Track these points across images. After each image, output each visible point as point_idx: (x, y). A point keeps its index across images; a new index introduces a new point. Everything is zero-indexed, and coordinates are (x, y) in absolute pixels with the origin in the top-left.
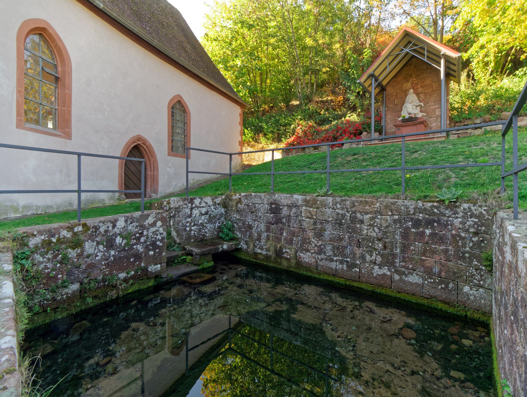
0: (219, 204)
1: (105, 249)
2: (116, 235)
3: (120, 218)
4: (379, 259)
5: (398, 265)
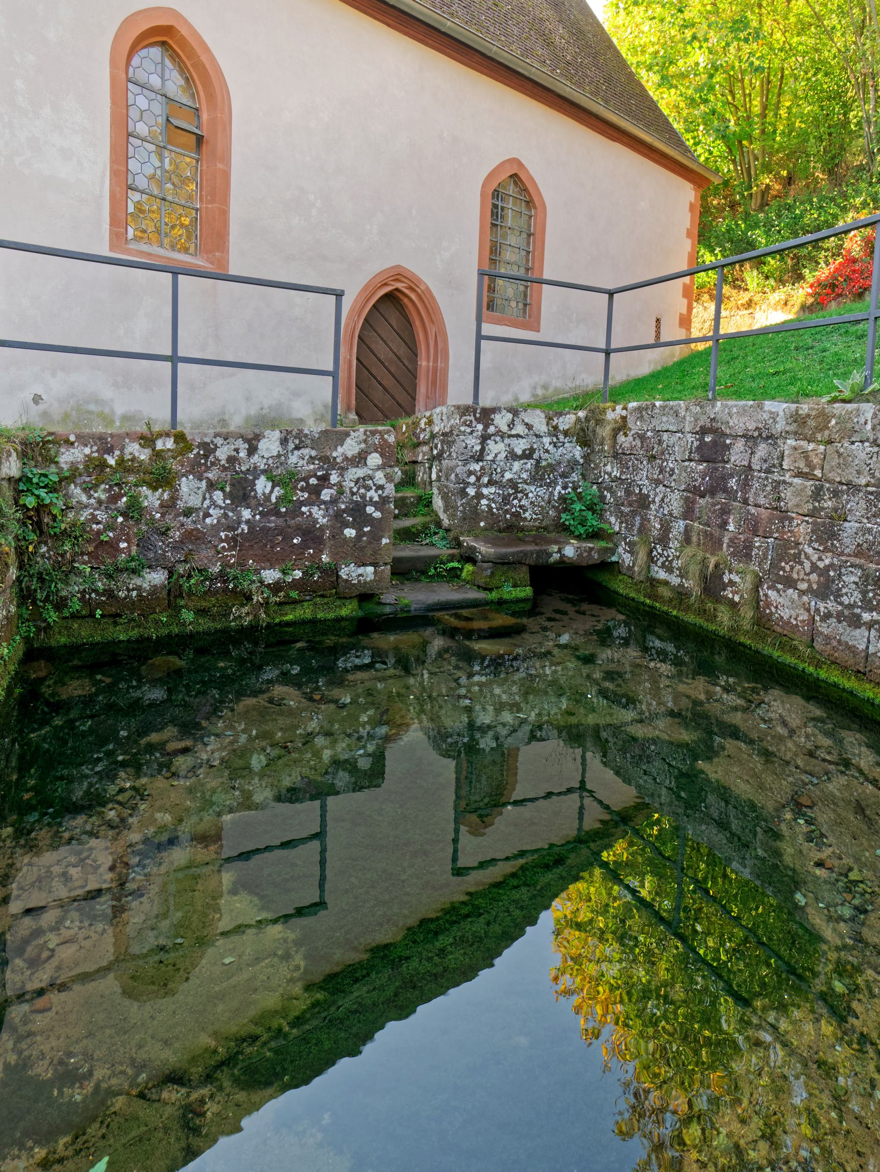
0: (566, 433)
1: (228, 502)
2: (255, 472)
3: (267, 433)
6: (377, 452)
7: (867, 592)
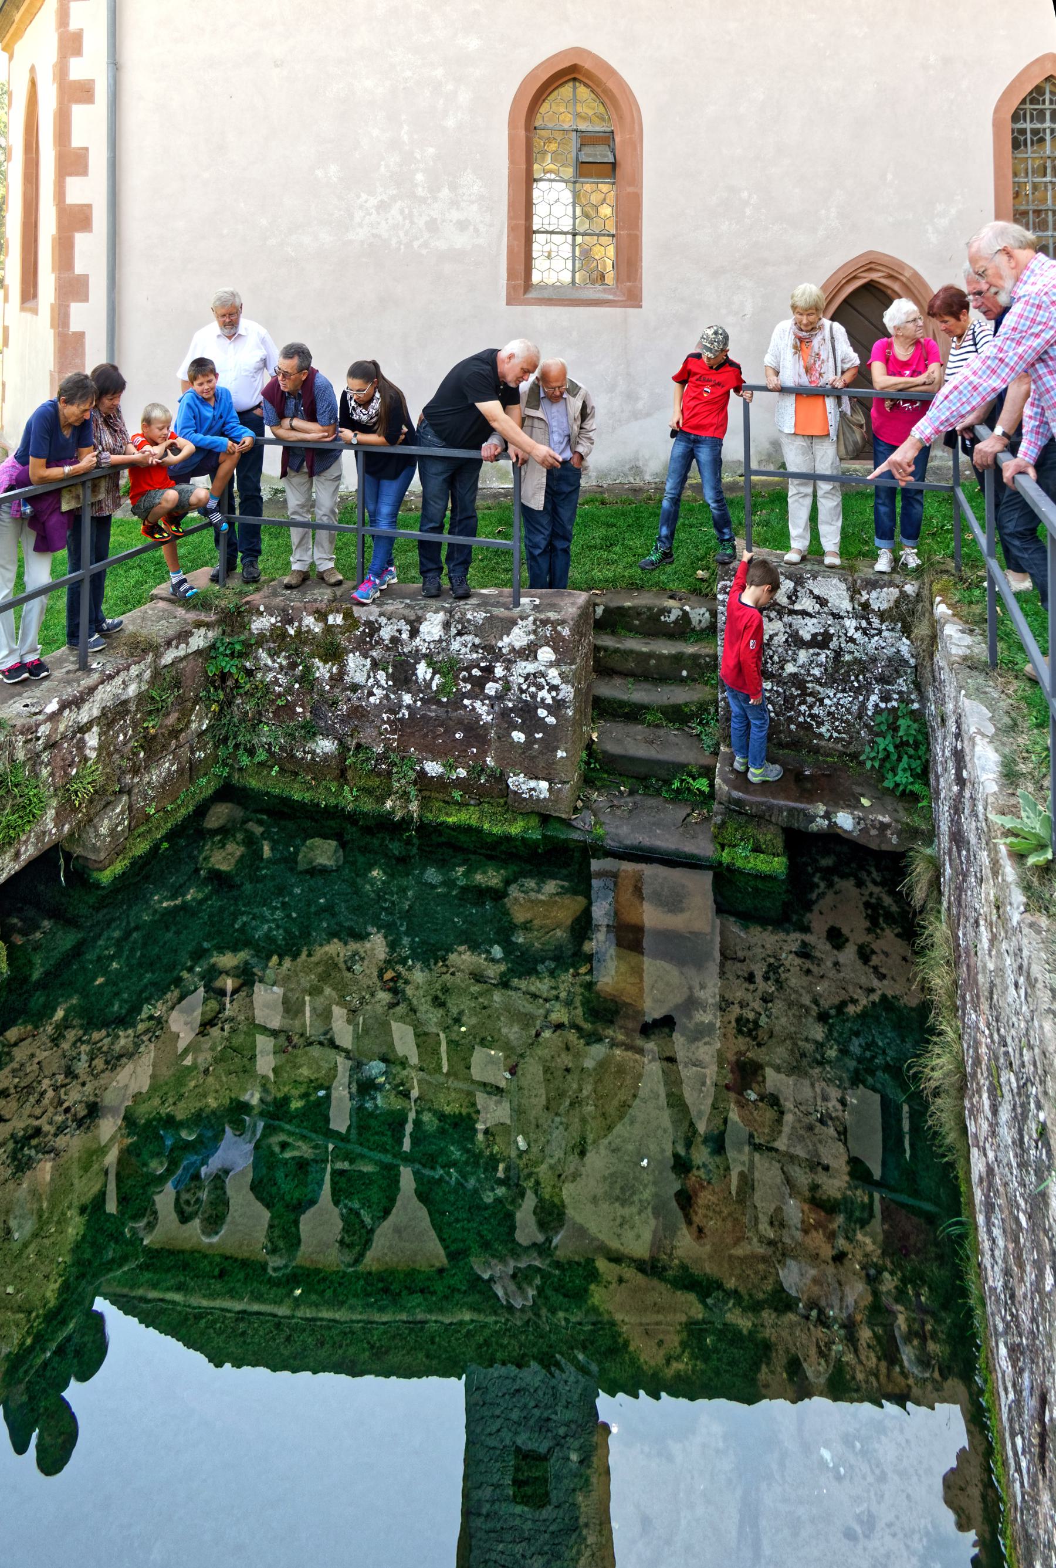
0: (882, 616)
3: (429, 615)
6: (547, 644)
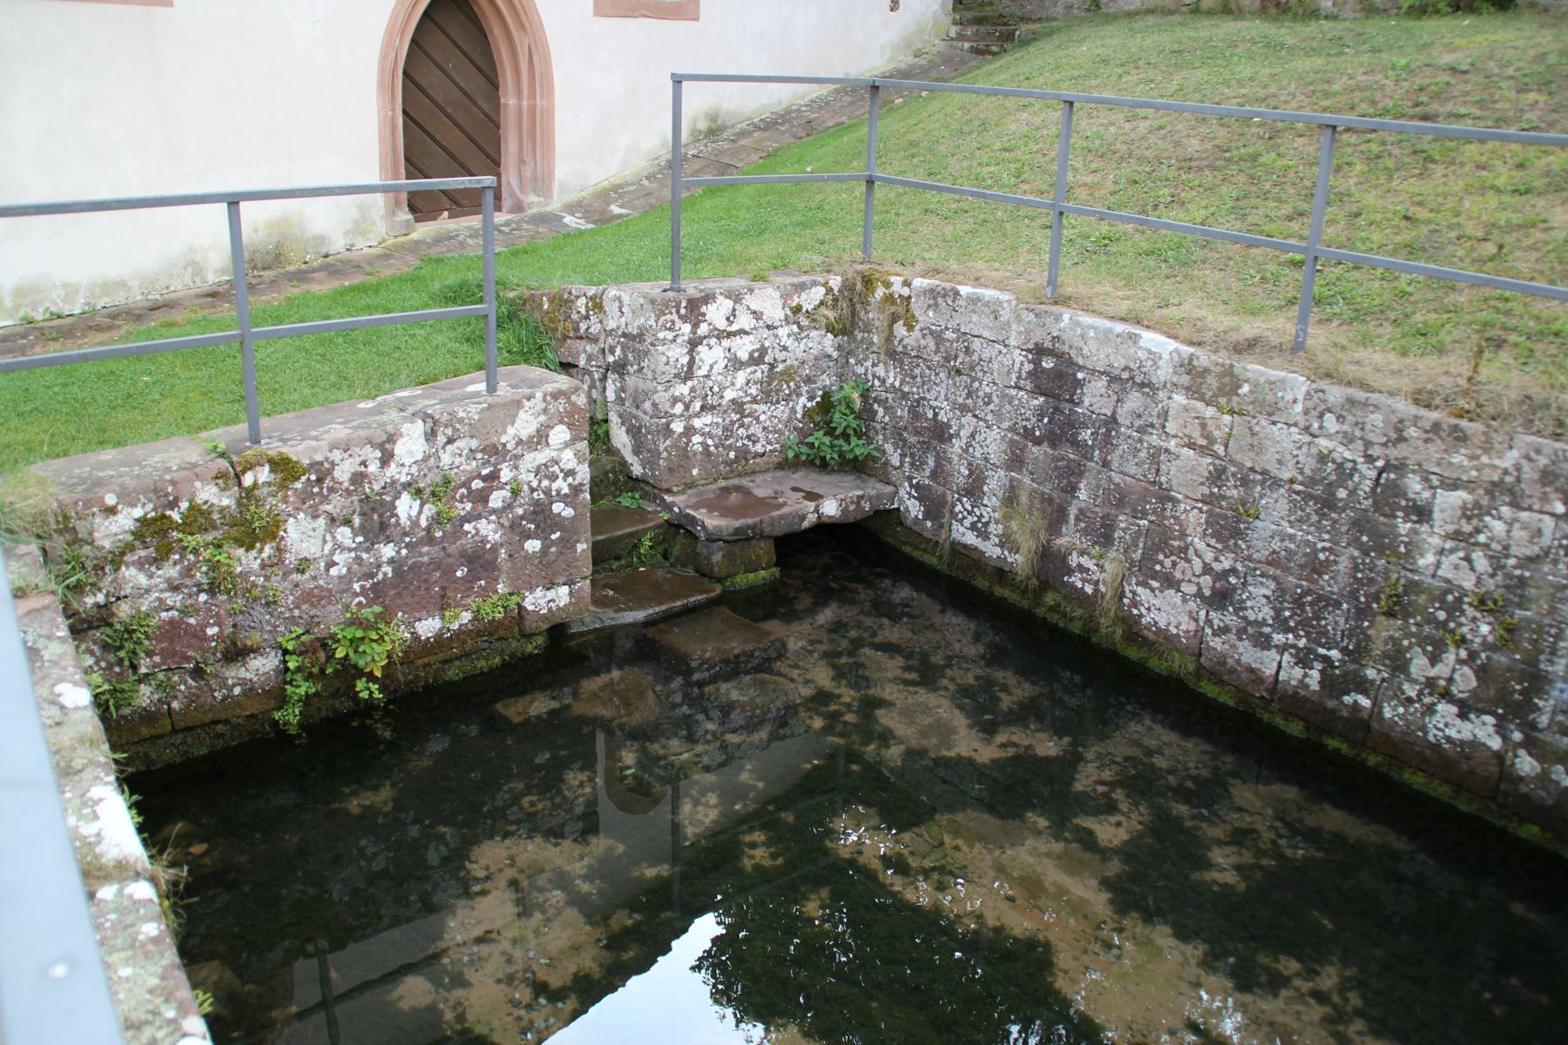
1: (360, 539)
2: (395, 488)
4: (1466, 681)
5: (1544, 720)
6: (561, 422)
7: (1284, 609)
